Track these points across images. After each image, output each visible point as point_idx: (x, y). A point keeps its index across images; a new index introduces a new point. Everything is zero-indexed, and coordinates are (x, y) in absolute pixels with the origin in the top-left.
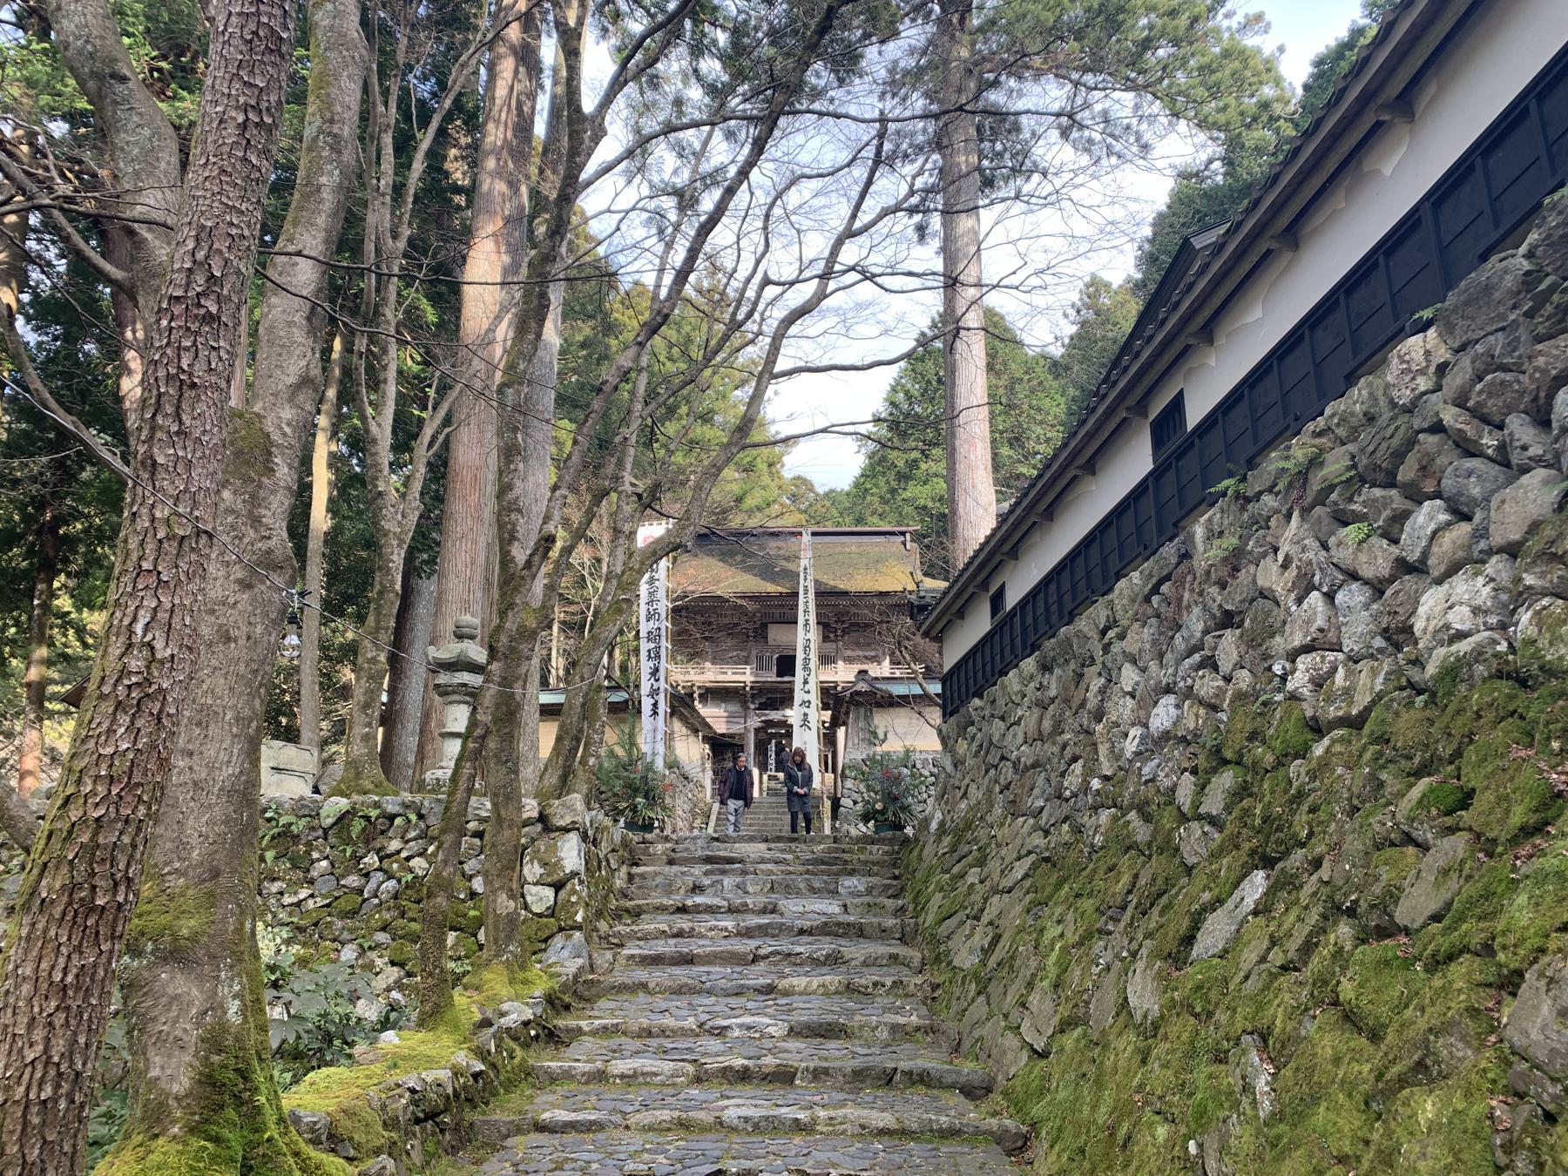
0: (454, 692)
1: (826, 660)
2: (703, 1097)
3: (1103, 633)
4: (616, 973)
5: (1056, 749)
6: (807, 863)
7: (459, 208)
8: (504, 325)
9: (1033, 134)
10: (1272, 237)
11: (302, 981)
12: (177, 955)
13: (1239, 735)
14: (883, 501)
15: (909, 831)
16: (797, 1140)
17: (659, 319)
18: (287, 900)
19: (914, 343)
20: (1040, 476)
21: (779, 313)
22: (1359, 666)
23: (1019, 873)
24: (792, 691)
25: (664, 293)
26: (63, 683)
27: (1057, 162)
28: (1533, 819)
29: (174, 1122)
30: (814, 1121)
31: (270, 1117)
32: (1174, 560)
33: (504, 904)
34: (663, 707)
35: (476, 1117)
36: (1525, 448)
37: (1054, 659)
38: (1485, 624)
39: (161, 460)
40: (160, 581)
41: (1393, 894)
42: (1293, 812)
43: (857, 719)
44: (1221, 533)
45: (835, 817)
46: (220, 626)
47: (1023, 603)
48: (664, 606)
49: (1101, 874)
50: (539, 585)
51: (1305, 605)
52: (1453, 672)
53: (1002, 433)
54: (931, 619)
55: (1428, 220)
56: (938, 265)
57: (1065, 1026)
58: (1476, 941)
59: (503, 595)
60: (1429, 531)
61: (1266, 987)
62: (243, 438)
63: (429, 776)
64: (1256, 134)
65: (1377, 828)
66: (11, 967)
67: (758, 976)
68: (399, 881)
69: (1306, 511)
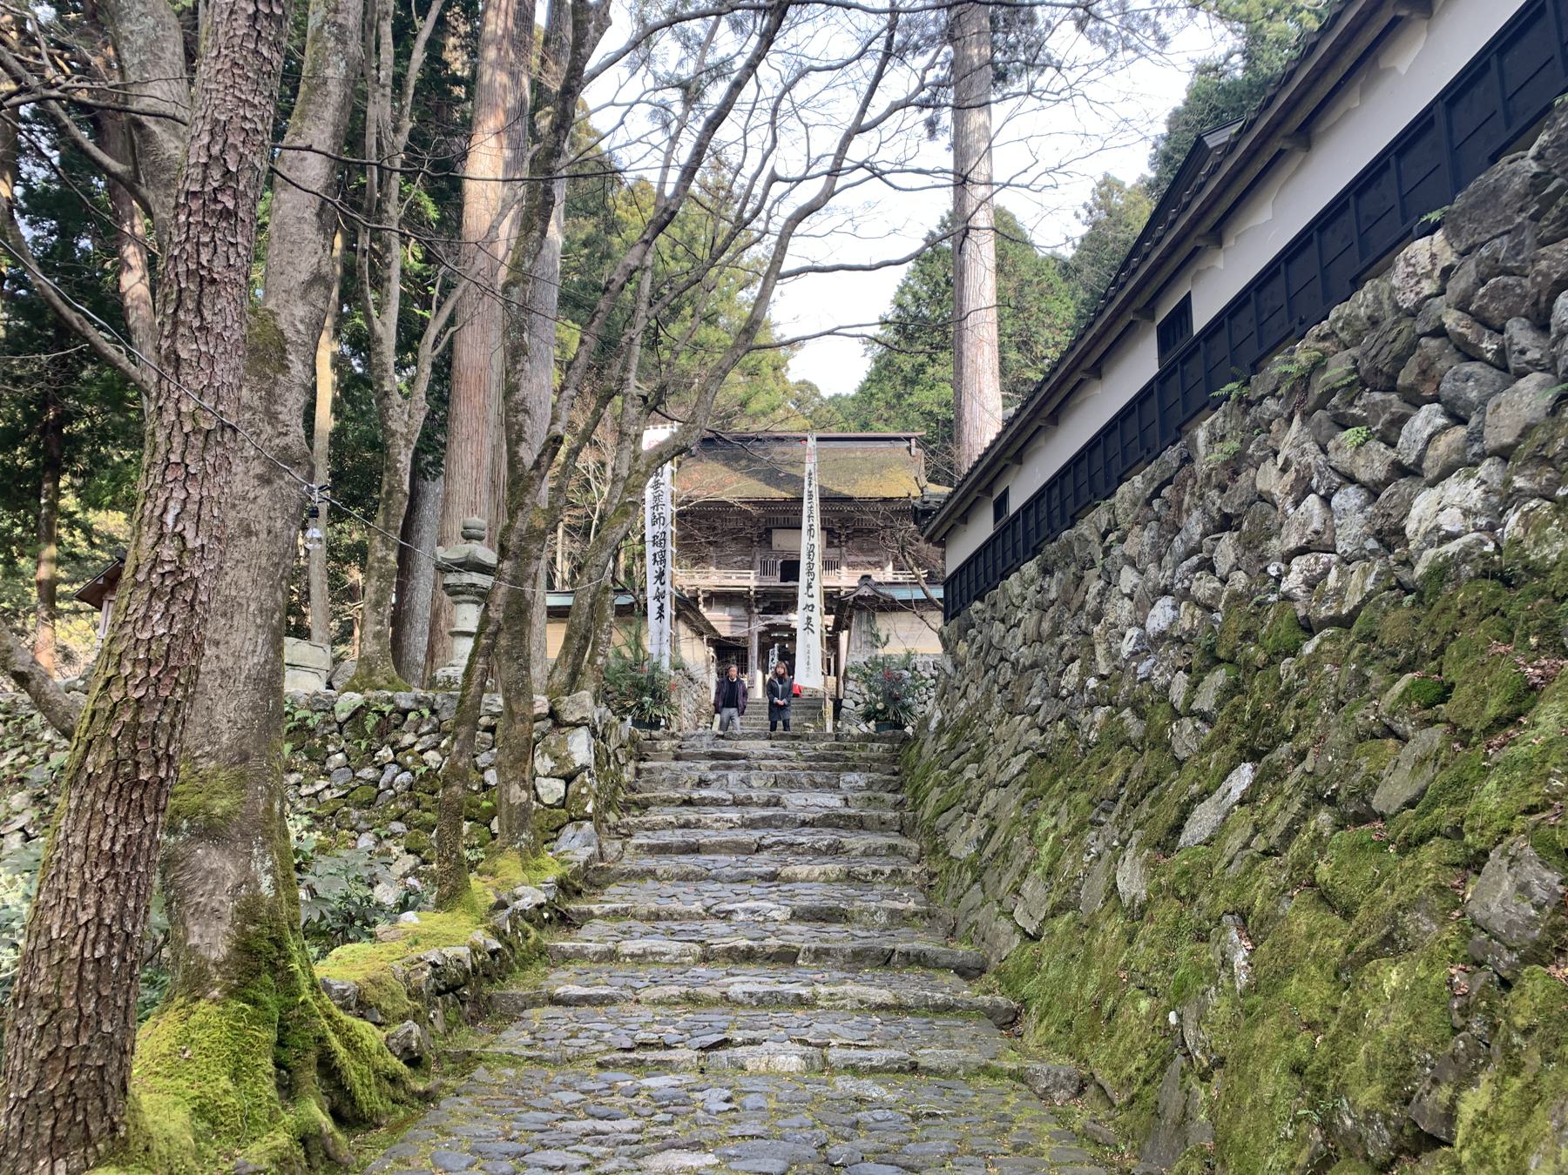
0: (462, 593)
1: (829, 565)
2: (709, 974)
3: (1104, 536)
4: (624, 861)
5: (1054, 650)
6: (809, 759)
7: (459, 100)
8: (506, 223)
9: (1048, 24)
10: (1285, 137)
11: (323, 865)
12: (211, 832)
13: (1232, 635)
14: (889, 406)
15: (909, 730)
16: (799, 1013)
17: (665, 216)
18: (305, 791)
19: (923, 243)
20: (1046, 380)
21: (787, 210)
22: (1351, 568)
23: (1015, 767)
24: (795, 596)
25: (669, 190)
26: (71, 582)
27: (1070, 57)
28: (1507, 711)
29: (213, 986)
30: (815, 996)
31: (304, 984)
32: (1175, 465)
33: (517, 794)
34: (669, 611)
35: (494, 991)
36: (1523, 352)
37: (1055, 563)
38: (1474, 525)
39: (184, 355)
40: (188, 473)
41: (1372, 783)
42: (1281, 708)
43: (860, 623)
44: (1223, 437)
45: (836, 716)
46: (241, 520)
47: (1026, 508)
48: (669, 510)
49: (1095, 768)
50: (547, 485)
51: (1302, 508)
52: (1440, 572)
53: (1010, 336)
54: (935, 523)
55: (1440, 121)
56: (948, 161)
57: (1056, 911)
58: (1446, 824)
59: (512, 495)
60: (1425, 435)
61: (1248, 871)
62: (258, 335)
63: (440, 673)
64: (1277, 26)
65: (1360, 721)
66: (62, 837)
67: (762, 864)
68: (413, 773)
69: (1306, 415)
